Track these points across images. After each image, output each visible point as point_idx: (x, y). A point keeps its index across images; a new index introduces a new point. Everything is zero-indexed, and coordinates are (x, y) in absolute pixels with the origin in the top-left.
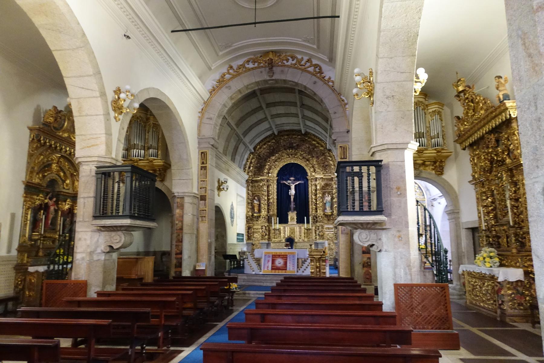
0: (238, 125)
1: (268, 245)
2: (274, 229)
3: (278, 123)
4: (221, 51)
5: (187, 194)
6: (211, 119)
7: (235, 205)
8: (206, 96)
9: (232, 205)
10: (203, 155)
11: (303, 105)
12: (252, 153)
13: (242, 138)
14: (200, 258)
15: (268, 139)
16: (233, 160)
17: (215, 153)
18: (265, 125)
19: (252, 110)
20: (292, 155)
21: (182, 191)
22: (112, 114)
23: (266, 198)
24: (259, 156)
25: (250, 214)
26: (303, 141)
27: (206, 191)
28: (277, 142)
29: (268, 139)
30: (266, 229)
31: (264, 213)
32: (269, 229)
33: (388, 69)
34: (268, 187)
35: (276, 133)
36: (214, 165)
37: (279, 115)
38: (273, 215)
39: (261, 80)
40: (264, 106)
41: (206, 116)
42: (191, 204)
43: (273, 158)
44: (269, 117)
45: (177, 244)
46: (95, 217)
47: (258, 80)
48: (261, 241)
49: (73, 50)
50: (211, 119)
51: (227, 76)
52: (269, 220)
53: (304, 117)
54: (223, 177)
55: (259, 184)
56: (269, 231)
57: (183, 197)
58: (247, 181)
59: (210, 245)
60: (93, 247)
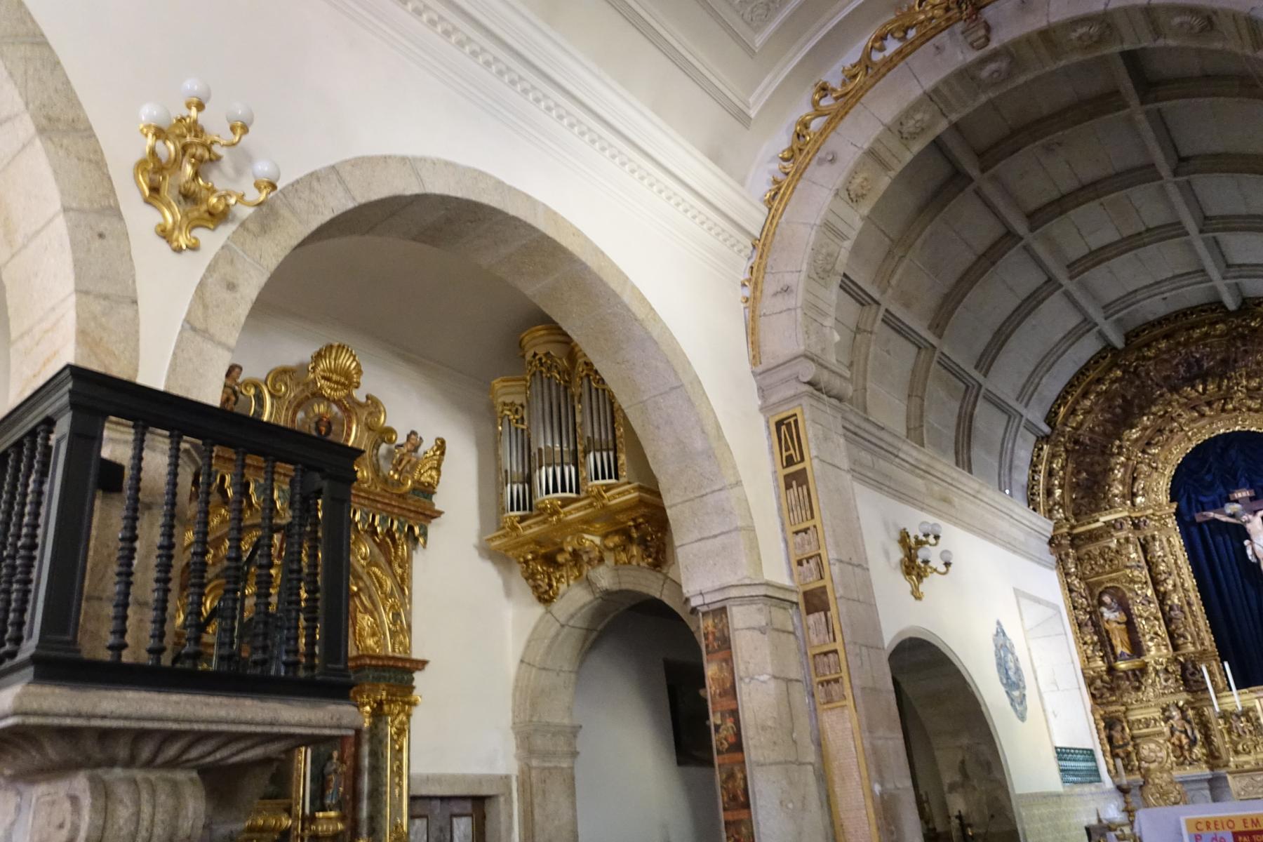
0: (938, 326)
1: (1216, 787)
2: (1225, 715)
3: (1112, 294)
4: (757, 30)
5: (734, 593)
6: (786, 290)
7: (1015, 634)
8: (755, 218)
9: (1000, 632)
10: (786, 432)
11: (1183, 160)
12: (1045, 439)
13: (980, 378)
15: (1092, 375)
16: (964, 460)
17: (839, 422)
18: (1054, 318)
19: (979, 258)
20: (1209, 404)
21: (717, 585)
22: (142, 219)
23: (1150, 592)
24: (1076, 442)
25: (1100, 664)
26: (1243, 337)
27: (820, 566)
28: (1132, 374)
29: (1092, 375)
30: (1184, 717)
31: (1156, 652)
32: (1200, 714)
34: (1145, 548)
35: (1119, 342)
36: (846, 466)
37: (1097, 257)
38: (1203, 655)
39: (943, 75)
40: (1021, 227)
41: (770, 286)
42: (762, 631)
43: (1135, 434)
44: (1062, 276)
45: (732, 816)
47: (929, 83)
48: (1178, 773)
50: (786, 290)
51: (816, 124)
52: (1189, 678)
53: (1207, 223)
54: (916, 521)
55: (1103, 543)
56: (1205, 726)
58: (1051, 542)
59: (886, 811)
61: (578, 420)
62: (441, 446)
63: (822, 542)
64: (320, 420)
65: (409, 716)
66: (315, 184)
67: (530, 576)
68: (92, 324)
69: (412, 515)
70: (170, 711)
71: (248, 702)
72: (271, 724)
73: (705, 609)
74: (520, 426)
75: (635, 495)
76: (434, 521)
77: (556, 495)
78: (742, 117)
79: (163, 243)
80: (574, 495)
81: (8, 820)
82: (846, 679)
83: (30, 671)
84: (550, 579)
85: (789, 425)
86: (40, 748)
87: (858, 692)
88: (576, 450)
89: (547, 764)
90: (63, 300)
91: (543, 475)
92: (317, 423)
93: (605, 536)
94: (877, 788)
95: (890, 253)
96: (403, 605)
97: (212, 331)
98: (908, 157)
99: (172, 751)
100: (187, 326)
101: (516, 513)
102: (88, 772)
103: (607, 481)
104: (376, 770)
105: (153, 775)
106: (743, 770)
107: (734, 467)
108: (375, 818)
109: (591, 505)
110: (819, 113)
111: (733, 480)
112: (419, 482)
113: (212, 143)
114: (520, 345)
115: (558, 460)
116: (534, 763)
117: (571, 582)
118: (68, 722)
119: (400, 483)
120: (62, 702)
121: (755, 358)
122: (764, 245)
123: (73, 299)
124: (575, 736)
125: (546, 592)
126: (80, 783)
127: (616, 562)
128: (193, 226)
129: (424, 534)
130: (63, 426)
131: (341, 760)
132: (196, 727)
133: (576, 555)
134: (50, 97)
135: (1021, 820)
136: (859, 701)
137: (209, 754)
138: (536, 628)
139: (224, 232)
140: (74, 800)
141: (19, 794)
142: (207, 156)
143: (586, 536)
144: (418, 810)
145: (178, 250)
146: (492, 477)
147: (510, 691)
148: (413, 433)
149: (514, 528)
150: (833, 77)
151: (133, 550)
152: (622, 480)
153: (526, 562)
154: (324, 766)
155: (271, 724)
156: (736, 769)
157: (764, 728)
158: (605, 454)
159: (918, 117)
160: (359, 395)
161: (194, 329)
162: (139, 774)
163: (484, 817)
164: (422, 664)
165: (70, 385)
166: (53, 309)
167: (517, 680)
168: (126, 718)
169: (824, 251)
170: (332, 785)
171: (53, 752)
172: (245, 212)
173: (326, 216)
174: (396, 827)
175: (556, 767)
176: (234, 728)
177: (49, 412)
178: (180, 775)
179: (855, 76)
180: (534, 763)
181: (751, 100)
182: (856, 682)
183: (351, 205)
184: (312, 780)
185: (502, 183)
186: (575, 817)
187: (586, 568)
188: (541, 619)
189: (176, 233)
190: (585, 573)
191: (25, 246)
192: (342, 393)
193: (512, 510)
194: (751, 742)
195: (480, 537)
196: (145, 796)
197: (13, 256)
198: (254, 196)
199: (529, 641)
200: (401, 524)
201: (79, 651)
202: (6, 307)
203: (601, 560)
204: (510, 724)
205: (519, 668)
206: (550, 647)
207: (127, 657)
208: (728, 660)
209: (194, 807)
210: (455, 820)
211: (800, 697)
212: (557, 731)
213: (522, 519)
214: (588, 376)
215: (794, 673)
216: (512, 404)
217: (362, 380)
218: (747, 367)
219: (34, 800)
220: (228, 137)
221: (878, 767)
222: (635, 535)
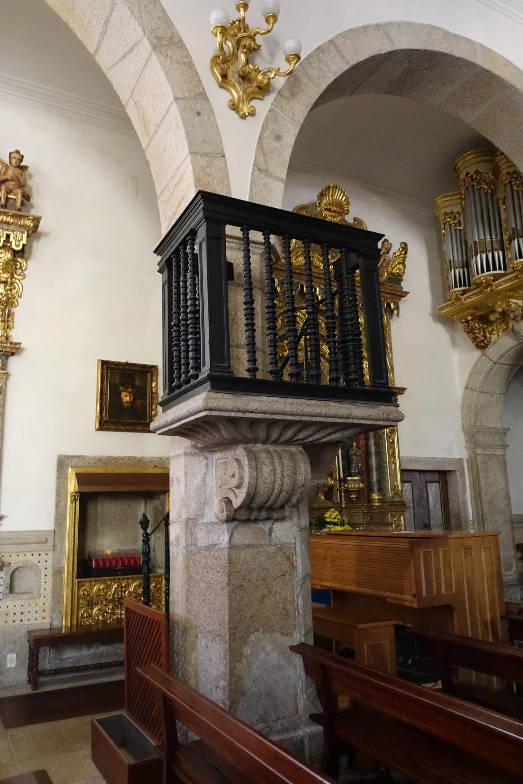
22: (220, 98)
60: (194, 505)
61: (503, 217)
62: (405, 247)
66: (321, 55)
67: (470, 331)
68: (202, 173)
69: (388, 296)
70: (288, 409)
71: (332, 404)
72: (347, 418)
76: (402, 299)
77: (489, 273)
80: (502, 272)
81: (203, 472)
83: (208, 385)
84: (485, 333)
86: (218, 430)
88: (502, 240)
89: (487, 453)
90: (183, 161)
97: (270, 170)
99: (289, 434)
100: (256, 168)
101: (459, 289)
102: (244, 446)
104: (379, 453)
105: (279, 448)
108: (381, 480)
109: (516, 277)
112: (391, 273)
113: (255, 35)
114: (456, 170)
115: (489, 248)
116: (479, 451)
117: (500, 333)
118: (233, 414)
120: (228, 403)
123: (189, 158)
126: (240, 451)
128: (251, 98)
129: (397, 308)
130: (202, 233)
131: (357, 447)
132: (304, 419)
133: (504, 314)
134: (156, 24)
137: (310, 436)
138: (475, 366)
139: (270, 99)
140: (238, 461)
141: (206, 458)
142: (253, 45)
143: (512, 300)
145: (243, 117)
146: (439, 266)
147: (459, 406)
151: (253, 309)
153: (467, 322)
154: (349, 451)
155: (347, 418)
161: (260, 170)
162: (271, 448)
163: (447, 483)
164: (402, 390)
165: (202, 205)
166: (178, 169)
167: (464, 400)
168: (264, 413)
170: (354, 461)
171: (226, 433)
172: (280, 82)
173: (331, 78)
174: (395, 487)
175: (493, 455)
176: (326, 420)
177: (192, 226)
178: (293, 449)
180: (479, 451)
183: (346, 67)
184: (342, 459)
186: (507, 486)
187: (511, 323)
188: (479, 360)
189: (241, 105)
190: (510, 327)
191: (156, 132)
193: (456, 287)
195: (433, 308)
196: (276, 460)
197: (150, 141)
198: (286, 67)
199: (471, 375)
201: (232, 372)
204: (461, 427)
205: (465, 392)
206: (486, 378)
207: (259, 376)
209: (304, 467)
210: (428, 484)
212: (494, 432)
213: (464, 292)
214: (510, 182)
216: (452, 213)
217: (351, 208)
219: (214, 462)
220: (266, 27)
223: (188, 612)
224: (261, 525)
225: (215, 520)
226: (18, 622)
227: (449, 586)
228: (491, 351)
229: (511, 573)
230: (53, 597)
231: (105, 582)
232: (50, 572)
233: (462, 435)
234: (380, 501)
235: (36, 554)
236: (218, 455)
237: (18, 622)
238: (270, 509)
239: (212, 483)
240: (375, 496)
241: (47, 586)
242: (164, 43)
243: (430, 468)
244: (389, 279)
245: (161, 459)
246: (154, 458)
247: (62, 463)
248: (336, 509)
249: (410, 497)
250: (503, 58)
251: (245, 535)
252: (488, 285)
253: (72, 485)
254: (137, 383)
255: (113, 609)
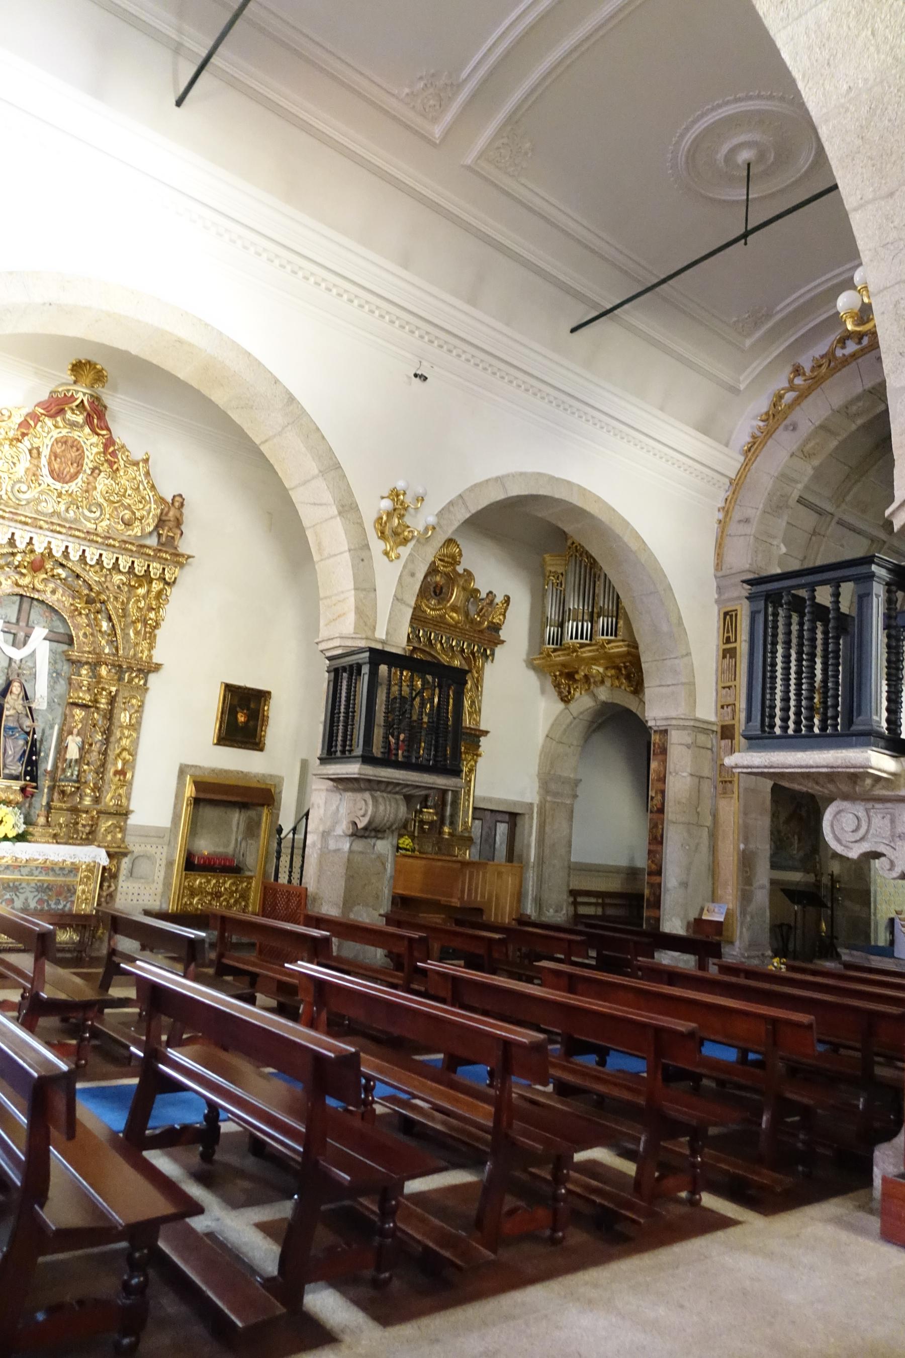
5: (674, 722)
6: (747, 521)
14: (720, 892)
21: (665, 715)
22: (377, 546)
27: (734, 711)
33: (894, 235)
41: (737, 515)
42: (688, 747)
46: (323, 760)
49: (280, 434)
50: (747, 521)
51: (789, 396)
57: (666, 731)
59: (746, 861)
60: (329, 824)
61: (597, 591)
62: (507, 600)
63: (738, 696)
64: (437, 586)
65: (476, 762)
67: (557, 686)
70: (401, 777)
73: (655, 728)
74: (559, 588)
75: (625, 649)
76: (499, 646)
78: (734, 390)
79: (385, 558)
80: (588, 642)
82: (736, 782)
84: (569, 688)
85: (731, 616)
87: (741, 790)
88: (593, 612)
91: (570, 626)
92: (434, 588)
93: (606, 668)
94: (742, 846)
95: (848, 476)
96: (477, 696)
98: (854, 427)
99: (397, 789)
103: (609, 637)
106: (662, 824)
107: (687, 644)
108: (454, 815)
109: (597, 650)
110: (792, 388)
111: (684, 652)
112: (492, 622)
115: (580, 618)
116: (549, 798)
119: (481, 623)
120: (371, 771)
121: (718, 566)
122: (737, 484)
124: (577, 786)
125: (567, 696)
126: (367, 795)
127: (612, 685)
129: (493, 654)
135: (875, 883)
136: (741, 796)
139: (411, 545)
140: (365, 801)
143: (594, 667)
144: (477, 816)
146: (538, 619)
148: (491, 592)
149: (549, 656)
150: (807, 365)
152: (619, 638)
153: (555, 676)
156: (659, 822)
157: (679, 803)
158: (610, 620)
159: (860, 404)
160: (460, 569)
161: (398, 599)
164: (486, 733)
167: (543, 746)
169: (779, 493)
174: (466, 823)
175: (562, 803)
178: (398, 797)
179: (820, 366)
180: (549, 798)
181: (741, 378)
182: (742, 785)
185: (554, 477)
188: (561, 712)
192: (449, 569)
194: (670, 810)
195: (528, 654)
199: (553, 725)
200: (479, 648)
202: (317, 582)
203: (602, 682)
205: (545, 741)
206: (565, 730)
208: (664, 762)
211: (707, 787)
212: (565, 781)
213: (555, 650)
215: (706, 772)
217: (462, 560)
218: (712, 570)
221: (746, 834)
222: (624, 672)
223: (318, 889)
224: (369, 840)
225: (342, 834)
226: (135, 901)
227: (483, 896)
228: (573, 705)
229: (561, 915)
230: (164, 884)
231: (206, 877)
232: (164, 863)
233: (537, 780)
234: (450, 834)
235: (154, 846)
236: (349, 794)
237: (135, 901)
238: (379, 831)
239: (343, 811)
240: (446, 829)
241: (160, 874)
242: (346, 508)
243: (501, 809)
244: (488, 627)
245: (263, 775)
246: (258, 774)
247: (183, 771)
248: (409, 837)
249: (479, 834)
250: (595, 495)
251: (359, 845)
252: (575, 651)
253: (189, 791)
254: (252, 706)
255: (210, 901)
